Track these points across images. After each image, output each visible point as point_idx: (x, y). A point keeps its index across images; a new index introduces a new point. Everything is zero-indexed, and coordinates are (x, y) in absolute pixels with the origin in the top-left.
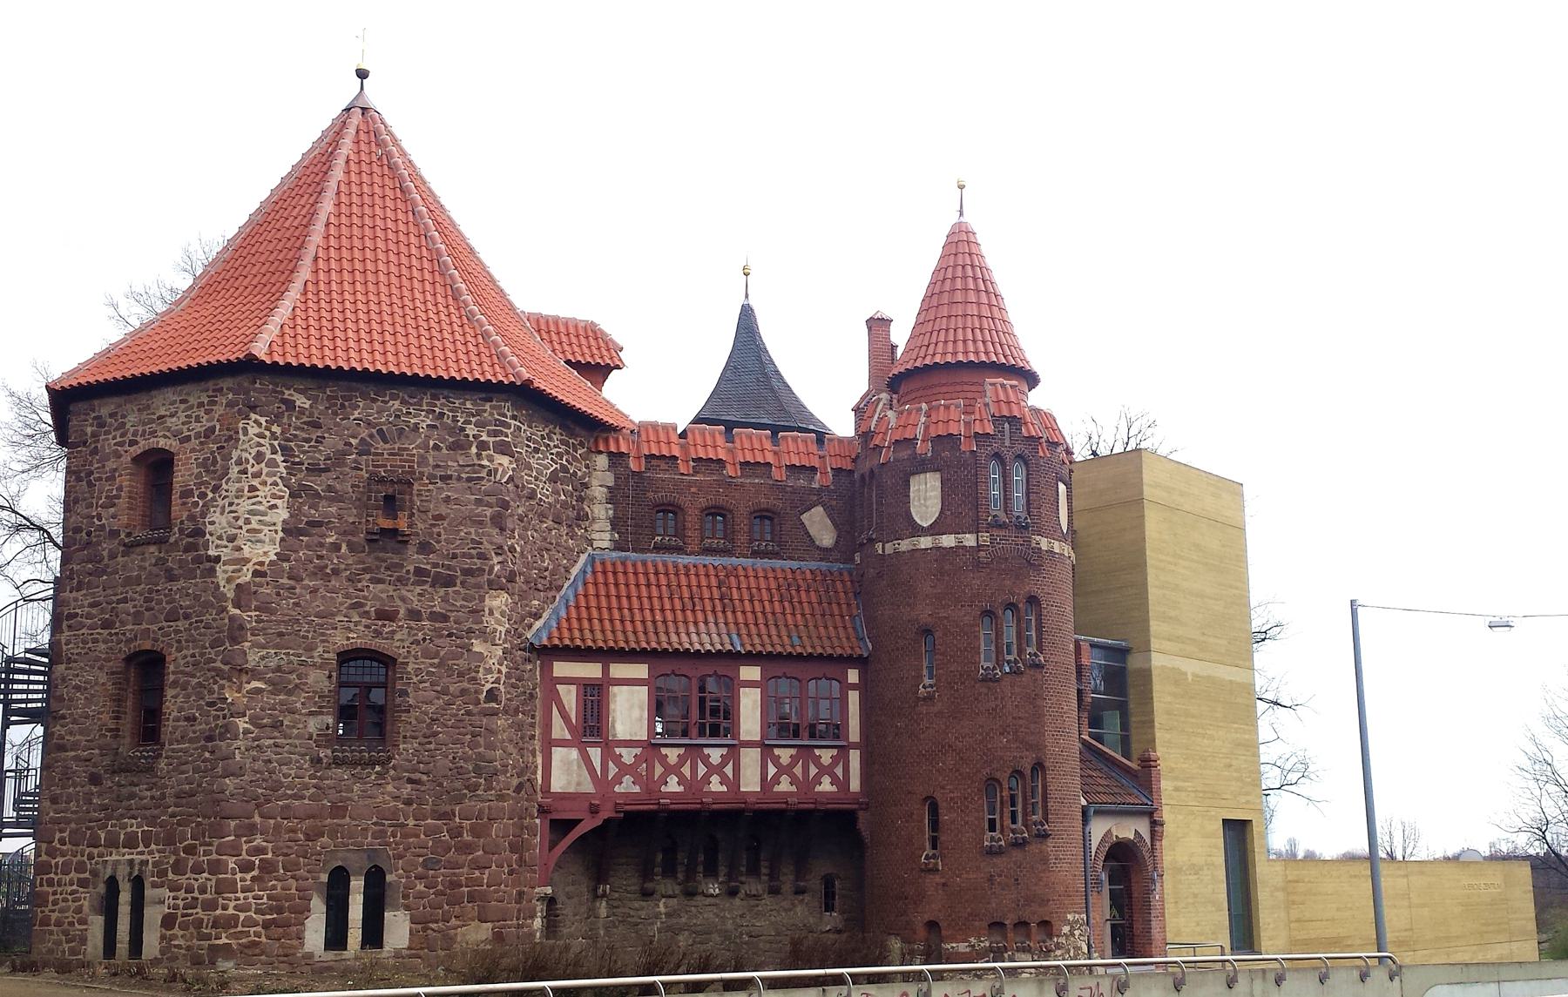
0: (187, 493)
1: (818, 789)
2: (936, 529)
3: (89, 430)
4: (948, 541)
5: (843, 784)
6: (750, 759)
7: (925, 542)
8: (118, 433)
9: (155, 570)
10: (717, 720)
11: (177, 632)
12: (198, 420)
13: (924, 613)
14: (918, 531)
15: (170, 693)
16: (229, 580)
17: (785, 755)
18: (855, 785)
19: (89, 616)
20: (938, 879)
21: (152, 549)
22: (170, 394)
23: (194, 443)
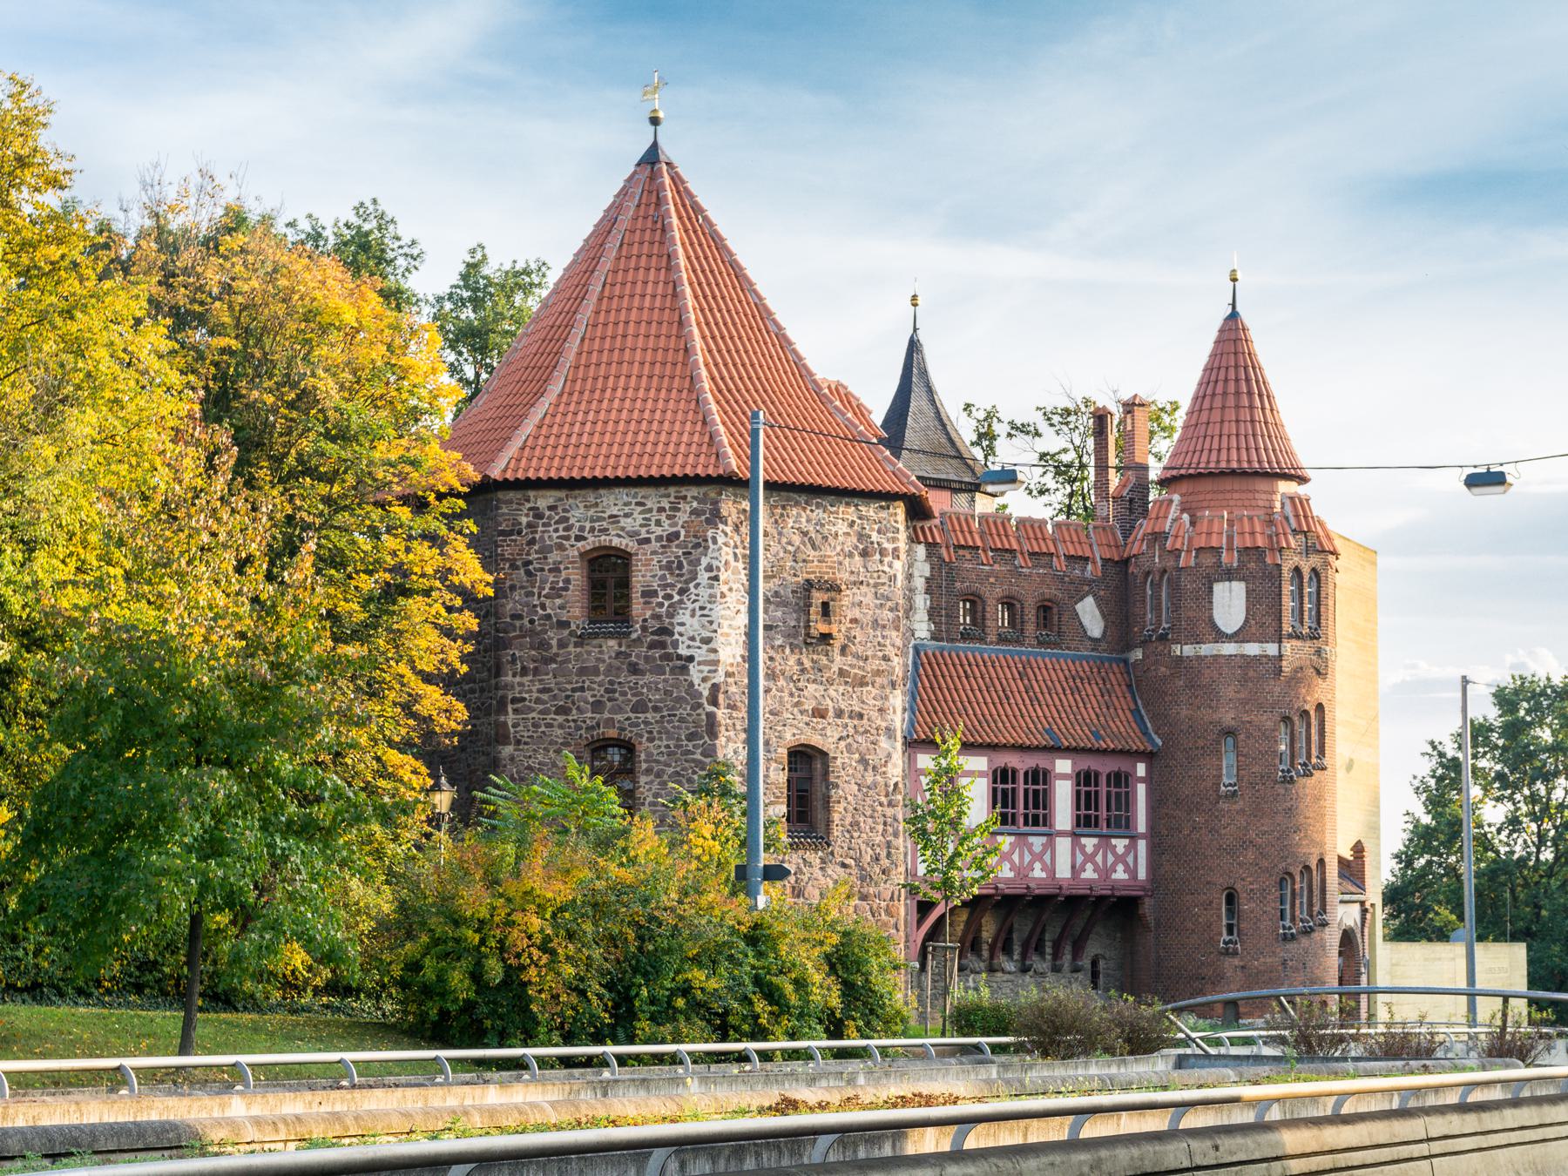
0: (649, 594)
1: (1114, 876)
2: (1239, 636)
3: (524, 520)
4: (1252, 649)
5: (1133, 872)
6: (1063, 845)
7: (1229, 649)
8: (561, 527)
9: (616, 663)
10: (1038, 814)
11: (646, 723)
12: (658, 523)
13: (1228, 717)
14: (1220, 636)
15: (643, 779)
16: (704, 680)
17: (1089, 843)
18: (1142, 874)
19: (538, 701)
20: (1236, 962)
21: (612, 643)
22: (623, 494)
23: (655, 545)
